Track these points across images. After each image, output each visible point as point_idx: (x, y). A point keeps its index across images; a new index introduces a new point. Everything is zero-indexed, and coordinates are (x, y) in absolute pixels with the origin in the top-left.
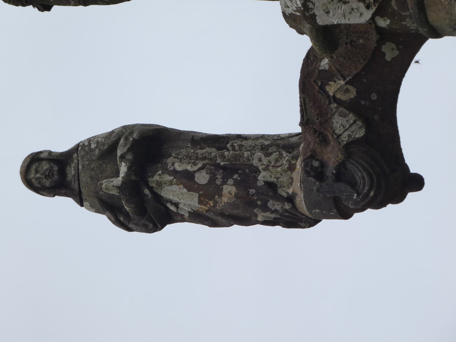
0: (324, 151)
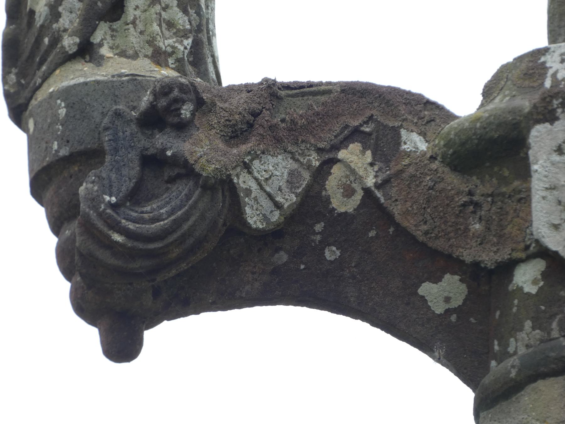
0: (214, 131)
